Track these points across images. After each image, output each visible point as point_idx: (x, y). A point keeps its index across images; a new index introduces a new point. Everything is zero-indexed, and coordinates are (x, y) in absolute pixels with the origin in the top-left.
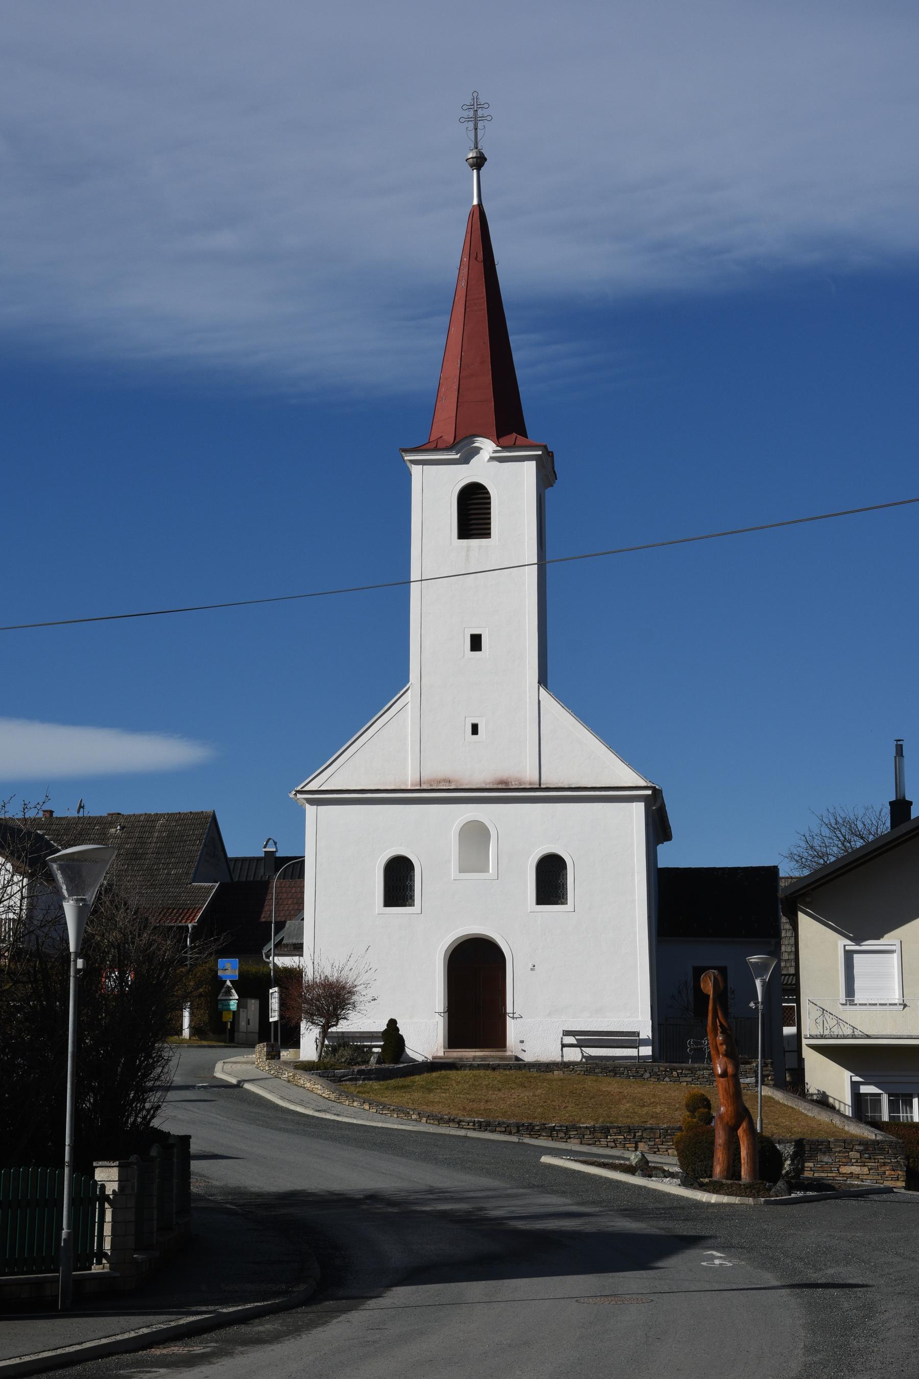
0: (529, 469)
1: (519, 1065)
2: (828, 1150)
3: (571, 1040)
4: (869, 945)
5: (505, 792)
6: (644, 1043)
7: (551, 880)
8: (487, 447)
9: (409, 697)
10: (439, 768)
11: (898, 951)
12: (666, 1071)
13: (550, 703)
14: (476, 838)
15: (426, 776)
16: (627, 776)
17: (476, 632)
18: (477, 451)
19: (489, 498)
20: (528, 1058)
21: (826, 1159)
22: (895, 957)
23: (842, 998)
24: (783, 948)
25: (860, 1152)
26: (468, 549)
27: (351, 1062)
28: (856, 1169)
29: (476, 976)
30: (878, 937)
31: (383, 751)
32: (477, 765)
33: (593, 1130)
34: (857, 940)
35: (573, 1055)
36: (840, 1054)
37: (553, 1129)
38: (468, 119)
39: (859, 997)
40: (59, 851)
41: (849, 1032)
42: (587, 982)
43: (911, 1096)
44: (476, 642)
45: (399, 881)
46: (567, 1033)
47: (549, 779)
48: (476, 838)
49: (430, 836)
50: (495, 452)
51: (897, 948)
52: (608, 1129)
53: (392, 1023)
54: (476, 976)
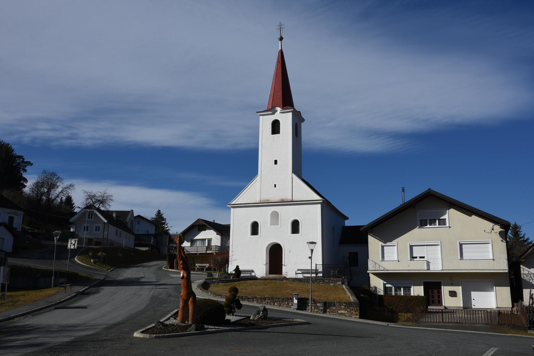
1: (285, 278)
2: (334, 305)
3: (300, 272)
4: (388, 244)
5: (283, 203)
6: (320, 272)
7: (295, 227)
8: (279, 109)
9: (258, 178)
10: (265, 197)
14: (275, 216)
15: (262, 199)
16: (316, 197)
18: (276, 111)
20: (288, 277)
21: (333, 308)
23: (381, 259)
25: (345, 306)
26: (274, 137)
27: (225, 278)
28: (343, 312)
29: (275, 253)
30: (391, 242)
31: (252, 192)
32: (276, 197)
33: (261, 299)
34: (385, 242)
35: (300, 276)
36: (380, 275)
37: (249, 298)
39: (386, 259)
41: (383, 269)
42: (304, 256)
43: (401, 287)
44: (276, 162)
45: (255, 228)
46: (298, 270)
47: (295, 199)
48: (275, 216)
49: (262, 215)
52: (265, 298)
54: (275, 253)
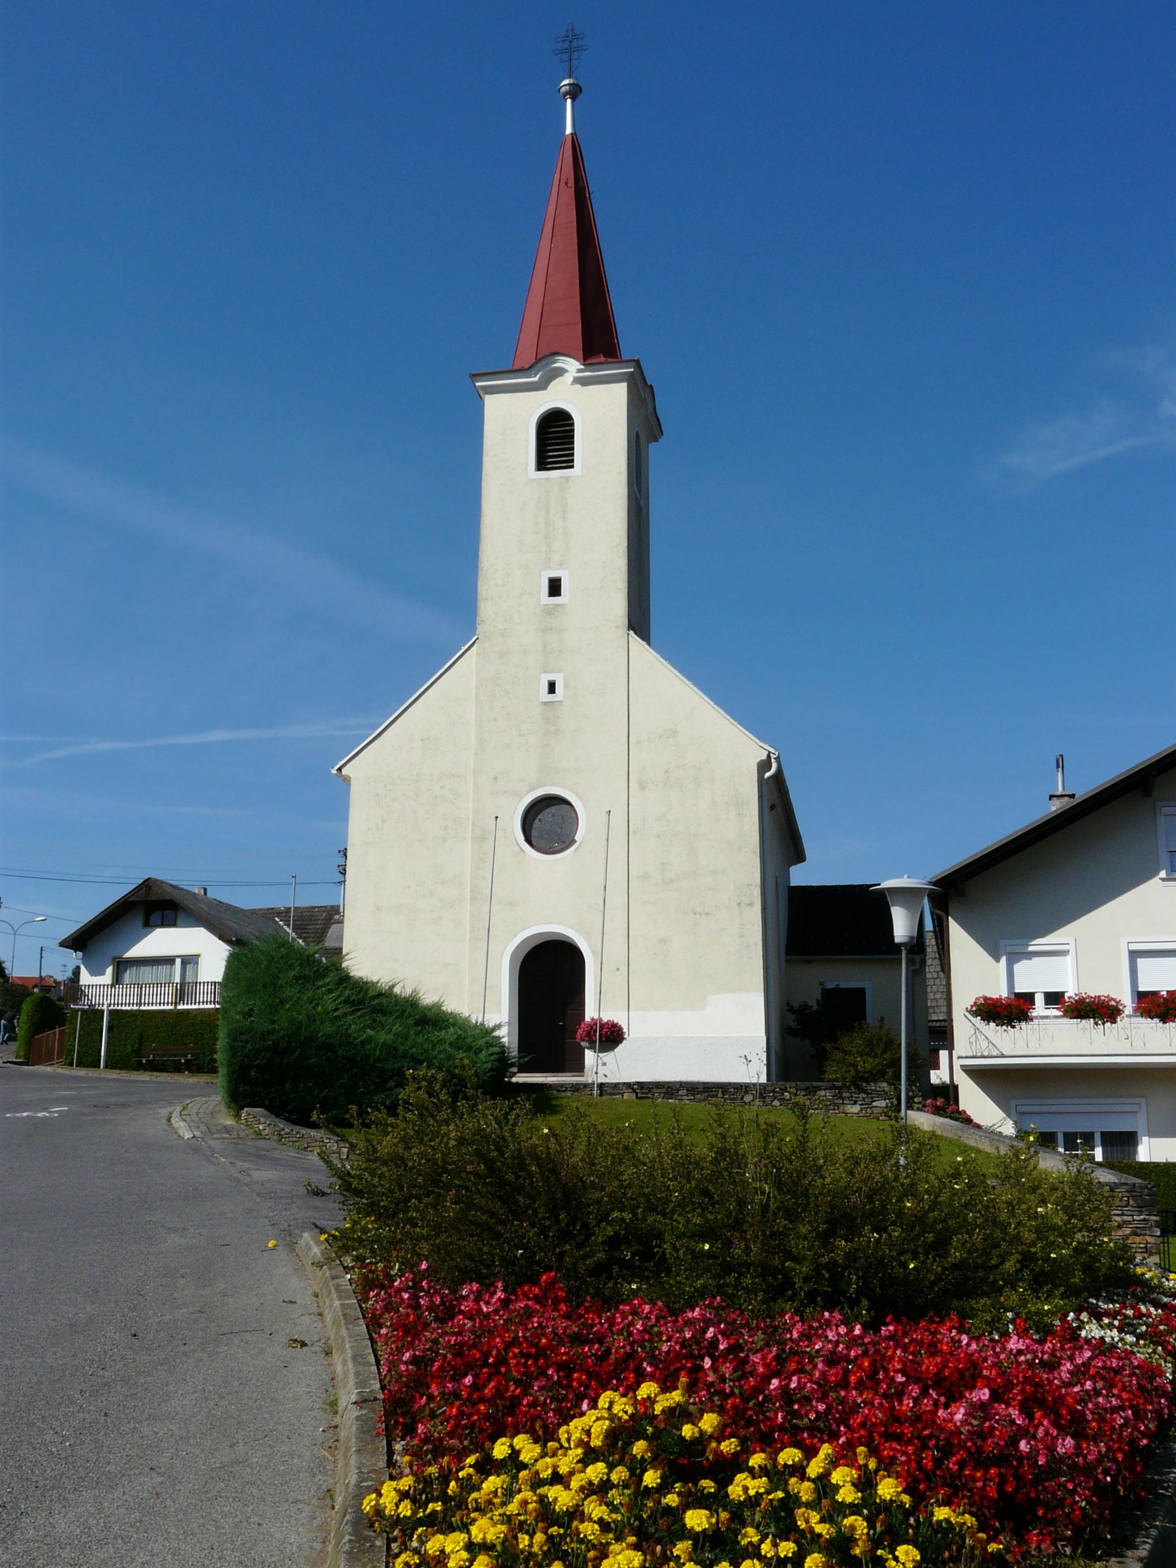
0: (619, 393)
8: (572, 366)
11: (1072, 952)
12: (773, 1091)
13: (631, 632)
17: (554, 574)
18: (561, 372)
19: (573, 425)
22: (1069, 960)
24: (928, 976)
38: (563, 51)
40: (288, 925)
50: (579, 371)
51: (1071, 948)
53: (63, 944)
